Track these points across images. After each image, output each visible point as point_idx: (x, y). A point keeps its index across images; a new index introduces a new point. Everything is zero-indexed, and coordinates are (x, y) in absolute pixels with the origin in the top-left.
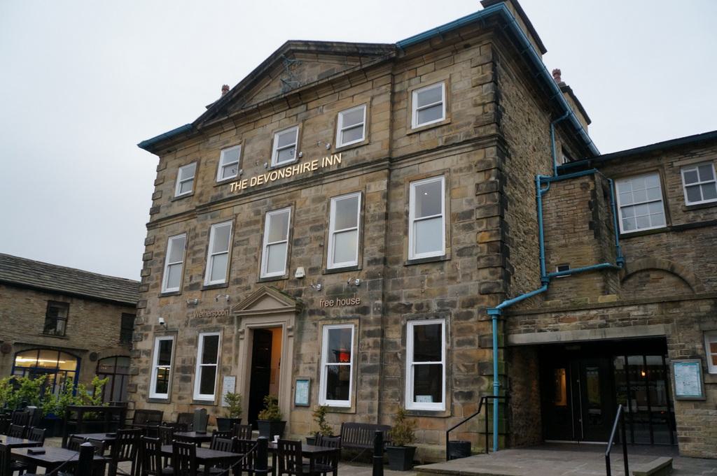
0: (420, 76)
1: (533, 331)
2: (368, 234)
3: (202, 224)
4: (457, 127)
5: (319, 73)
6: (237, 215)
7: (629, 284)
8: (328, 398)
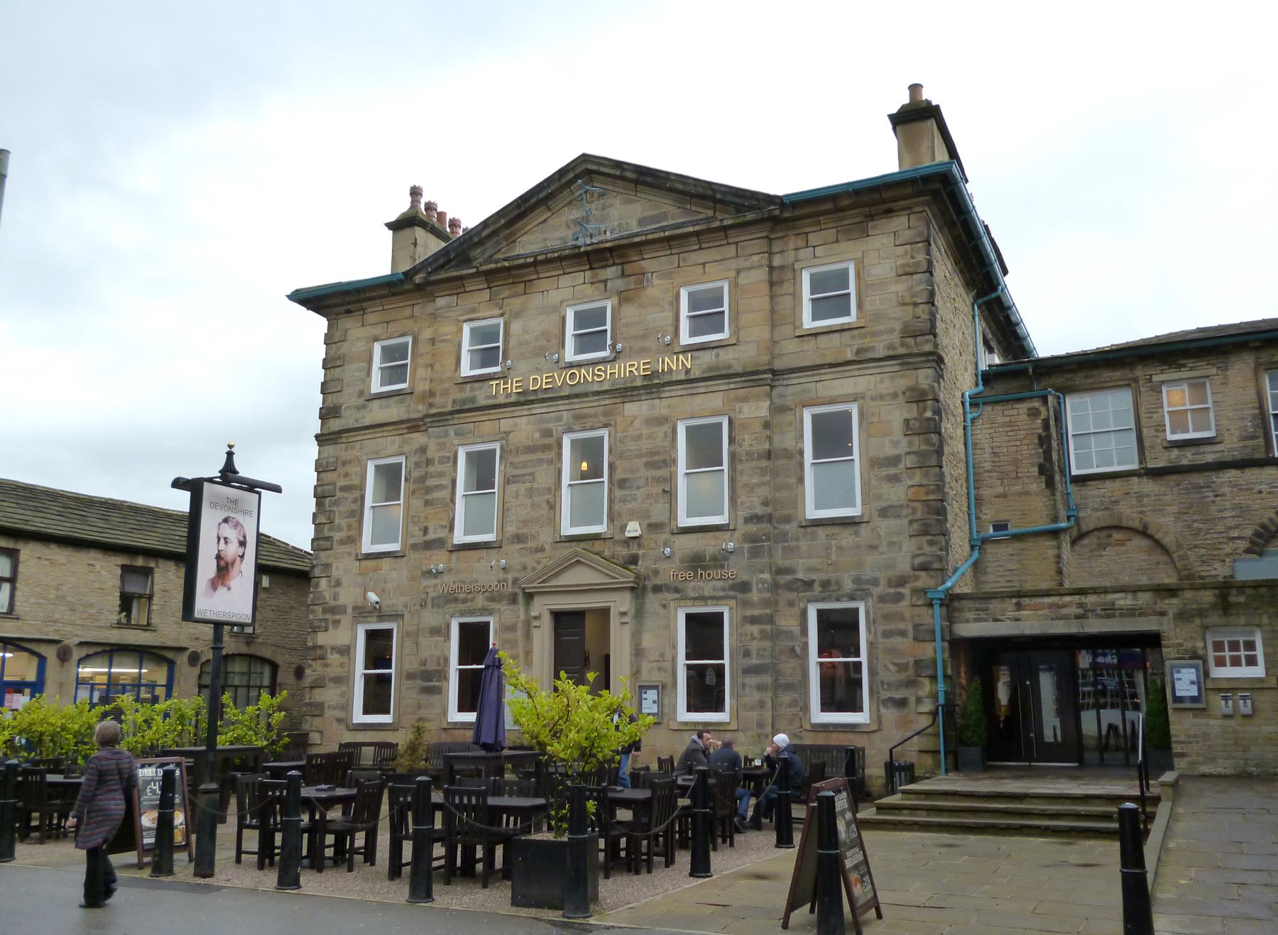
0: (814, 247)
1: (987, 620)
2: (742, 480)
3: (438, 444)
4: (874, 334)
5: (640, 216)
6: (508, 433)
7: (1083, 546)
8: (689, 710)
